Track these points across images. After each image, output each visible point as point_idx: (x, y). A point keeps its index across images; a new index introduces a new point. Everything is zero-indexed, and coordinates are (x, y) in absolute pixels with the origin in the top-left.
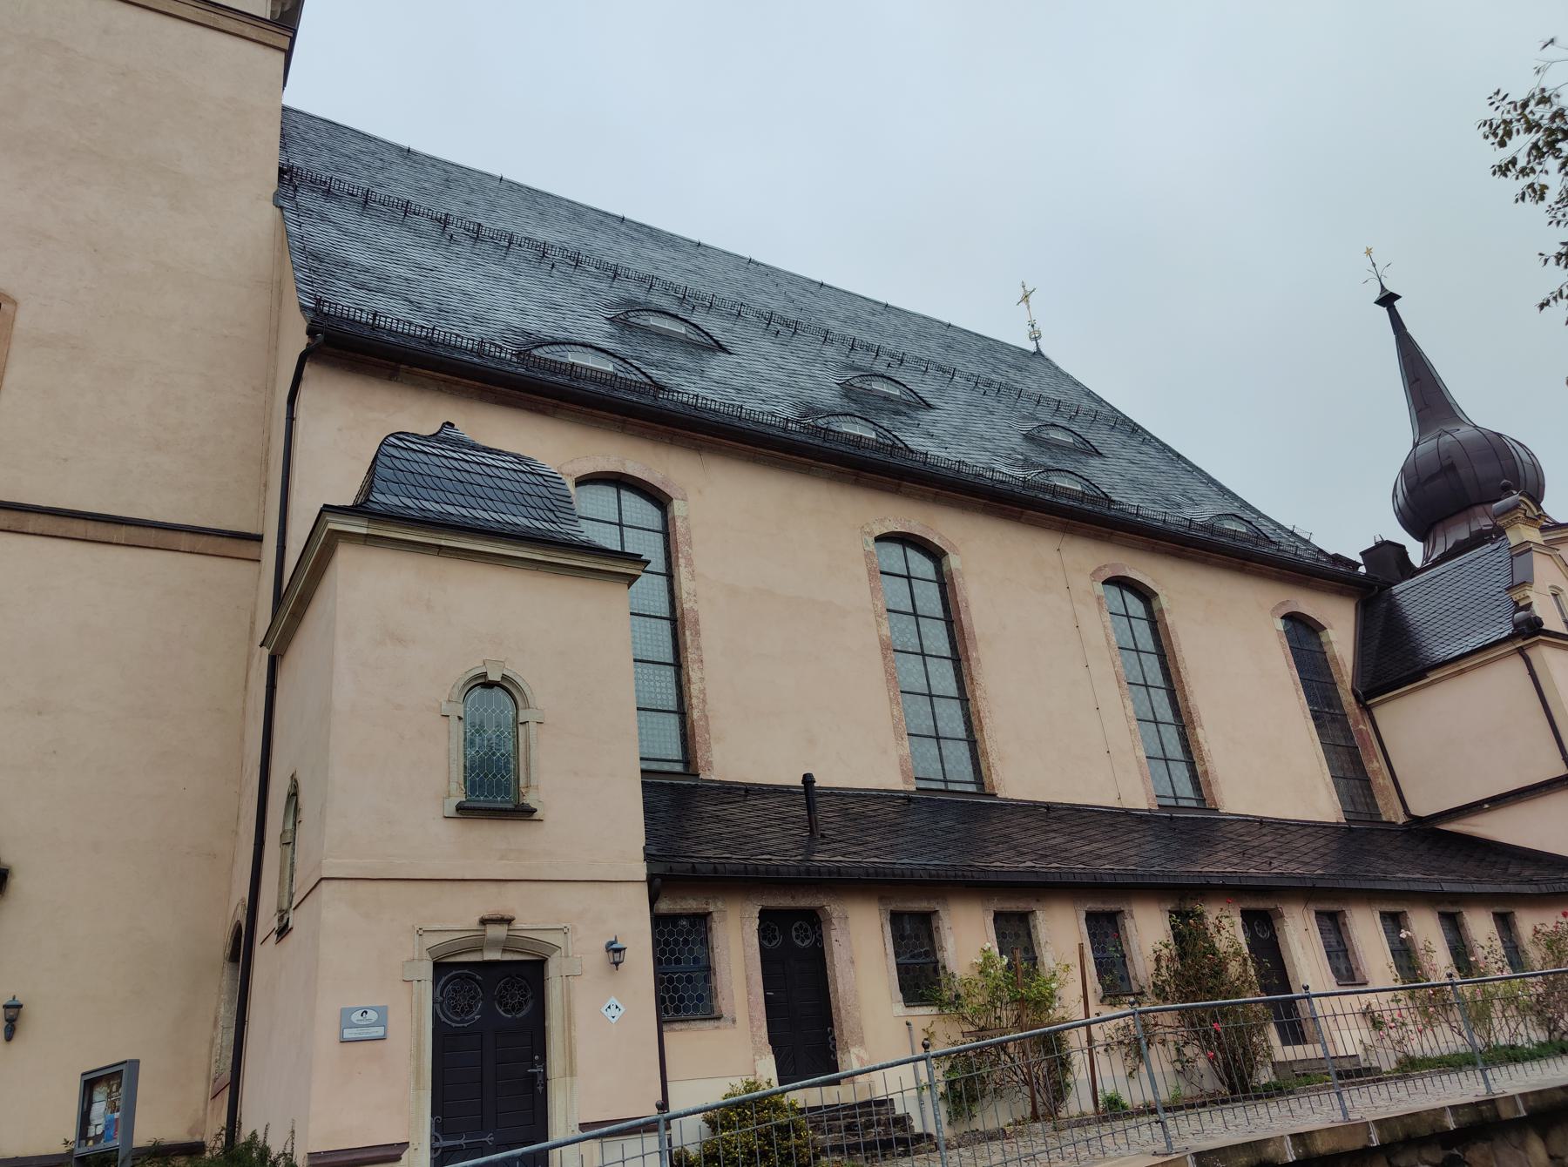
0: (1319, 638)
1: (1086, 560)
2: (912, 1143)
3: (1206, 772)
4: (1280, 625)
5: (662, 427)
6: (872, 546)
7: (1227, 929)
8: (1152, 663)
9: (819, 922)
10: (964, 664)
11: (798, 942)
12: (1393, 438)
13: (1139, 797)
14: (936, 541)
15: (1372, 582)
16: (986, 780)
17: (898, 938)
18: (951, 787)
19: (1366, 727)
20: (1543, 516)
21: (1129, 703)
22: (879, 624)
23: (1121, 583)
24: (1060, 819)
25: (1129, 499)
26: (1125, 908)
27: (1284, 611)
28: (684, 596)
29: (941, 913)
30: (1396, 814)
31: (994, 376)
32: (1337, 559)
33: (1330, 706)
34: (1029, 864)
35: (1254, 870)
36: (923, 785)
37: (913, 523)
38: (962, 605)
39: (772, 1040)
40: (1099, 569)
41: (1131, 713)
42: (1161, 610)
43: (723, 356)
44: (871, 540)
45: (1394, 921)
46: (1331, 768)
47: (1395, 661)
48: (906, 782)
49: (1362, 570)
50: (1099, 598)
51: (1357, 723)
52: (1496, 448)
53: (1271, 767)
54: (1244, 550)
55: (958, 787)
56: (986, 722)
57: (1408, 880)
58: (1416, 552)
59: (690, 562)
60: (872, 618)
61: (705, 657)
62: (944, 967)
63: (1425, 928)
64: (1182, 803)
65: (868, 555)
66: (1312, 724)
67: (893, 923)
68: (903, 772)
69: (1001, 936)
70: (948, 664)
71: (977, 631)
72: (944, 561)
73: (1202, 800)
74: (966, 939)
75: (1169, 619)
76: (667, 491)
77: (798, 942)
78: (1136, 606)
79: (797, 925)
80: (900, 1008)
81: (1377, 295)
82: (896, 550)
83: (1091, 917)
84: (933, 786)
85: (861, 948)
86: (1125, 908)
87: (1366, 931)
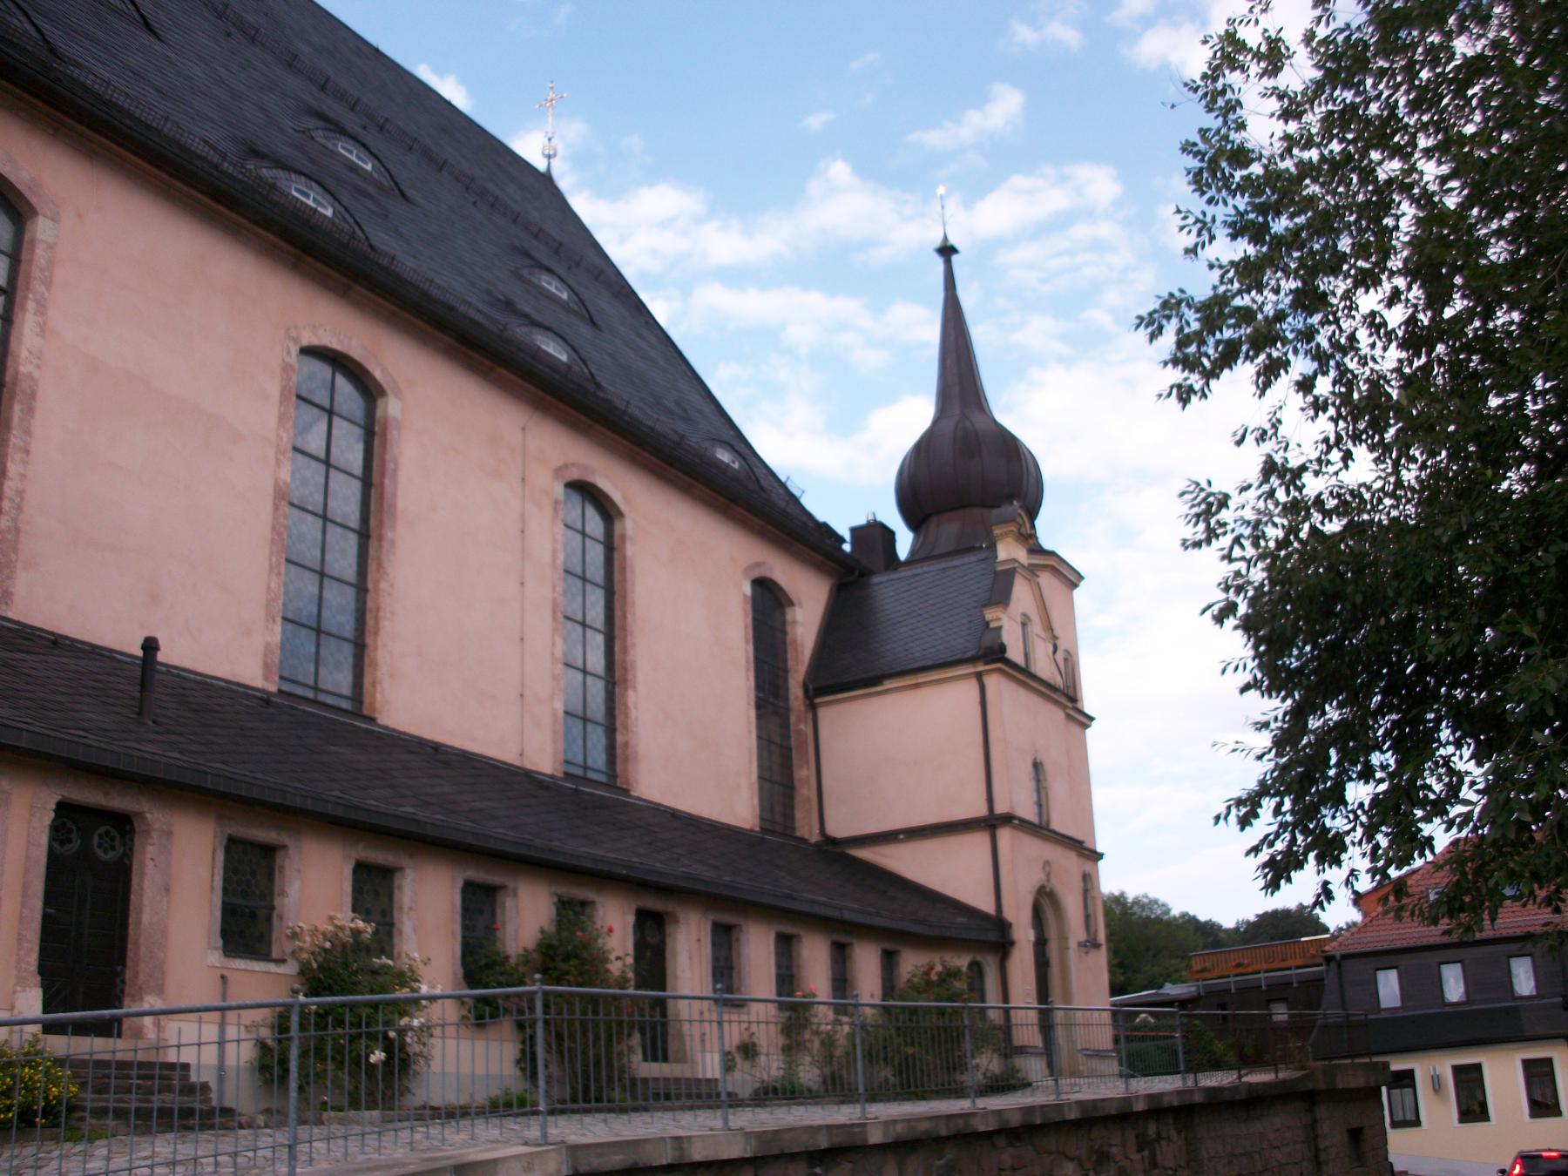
0: (783, 614)
1: (554, 450)
2: (217, 1118)
3: (626, 745)
4: (747, 589)
5: (43, 107)
6: (294, 358)
7: (614, 926)
8: (596, 599)
9: (133, 831)
10: (373, 544)
11: (100, 852)
12: (913, 416)
13: (543, 757)
14: (378, 374)
15: (854, 564)
16: (367, 699)
17: (231, 871)
18: (322, 698)
19: (807, 728)
20: (1033, 536)
21: (559, 641)
22: (278, 464)
23: (585, 491)
24: (447, 764)
25: (616, 389)
26: (510, 883)
27: (757, 573)
28: (24, 354)
29: (291, 850)
30: (811, 832)
31: (490, 186)
32: (825, 529)
33: (776, 696)
34: (410, 810)
35: (658, 865)
36: (287, 687)
37: (354, 342)
38: (390, 466)
39: (43, 970)
40: (566, 466)
41: (559, 652)
42: (623, 537)
43: (148, 40)
44: (295, 350)
45: (785, 943)
46: (761, 767)
47: (854, 659)
48: (266, 678)
49: (847, 547)
50: (556, 502)
51: (799, 721)
52: (1010, 449)
53: (695, 753)
54: (752, 500)
55: (330, 700)
56: (385, 624)
57: (814, 902)
58: (904, 541)
59: (42, 308)
60: (271, 453)
61: (34, 448)
62: (281, 917)
63: (815, 956)
64: (591, 775)
65: (287, 368)
66: (753, 713)
67: (228, 850)
68: (266, 665)
69: (358, 891)
70: (353, 539)
71: (401, 504)
72: (380, 403)
73: (612, 773)
74: (315, 891)
75: (630, 549)
76: (33, 200)
77: (100, 852)
78: (595, 524)
79: (102, 829)
80: (216, 958)
81: (938, 242)
82: (323, 370)
83: (469, 888)
84: (300, 691)
85: (179, 874)
86: (510, 883)
87: (757, 950)
